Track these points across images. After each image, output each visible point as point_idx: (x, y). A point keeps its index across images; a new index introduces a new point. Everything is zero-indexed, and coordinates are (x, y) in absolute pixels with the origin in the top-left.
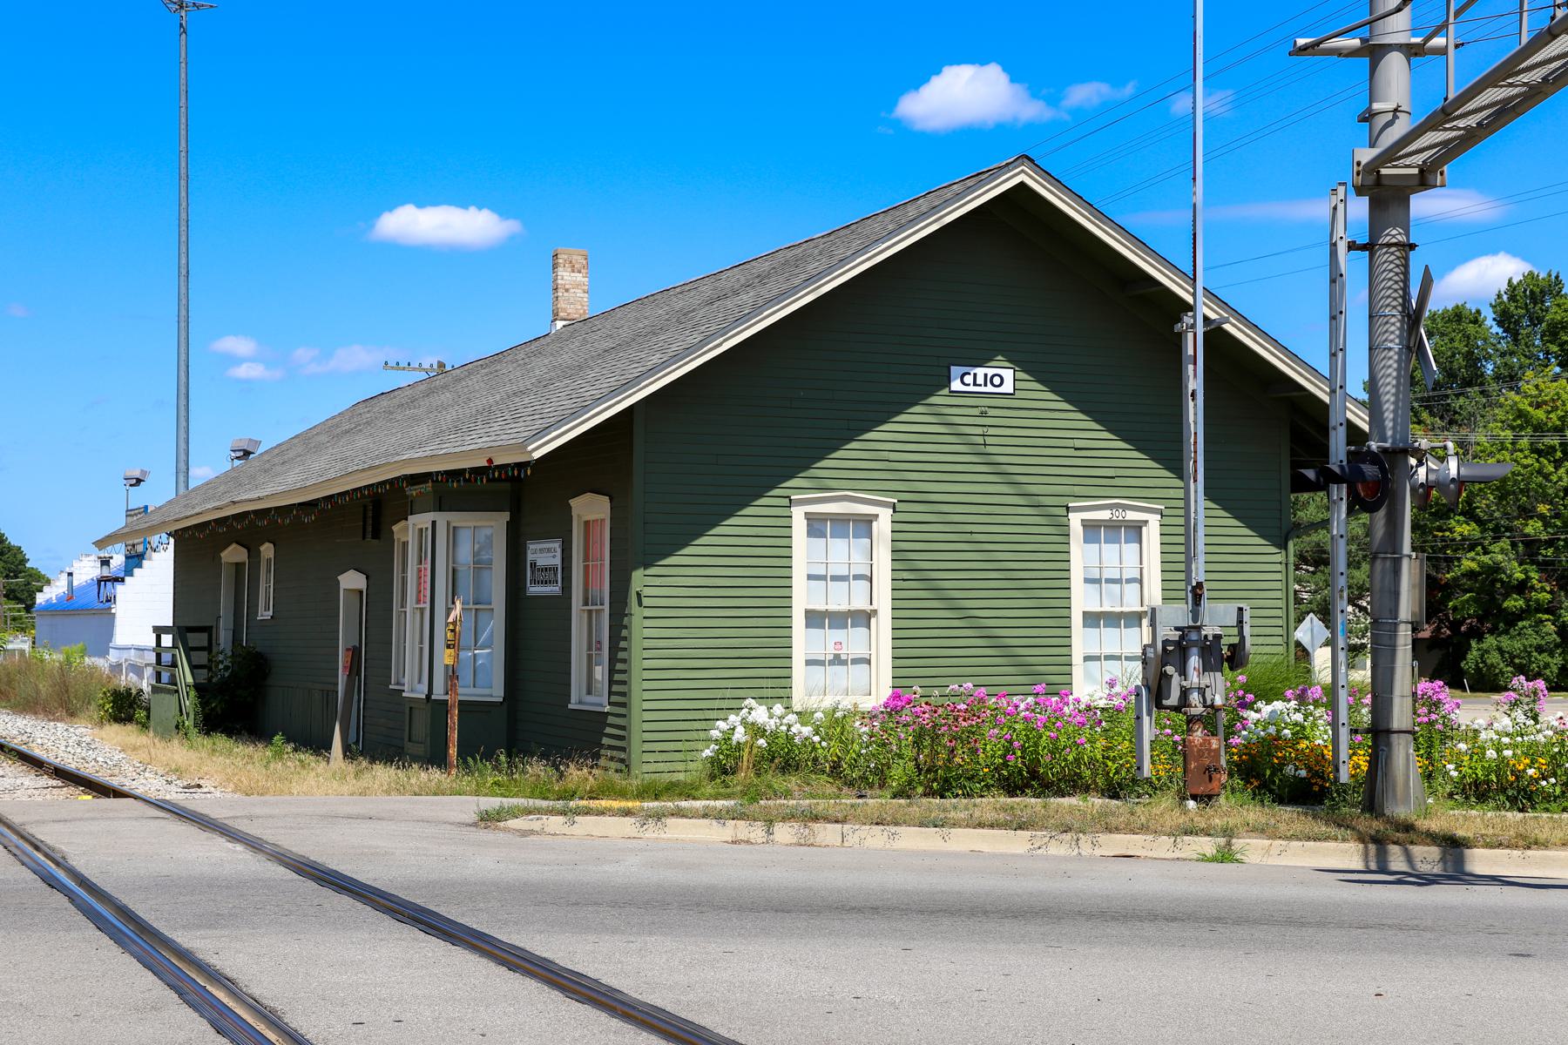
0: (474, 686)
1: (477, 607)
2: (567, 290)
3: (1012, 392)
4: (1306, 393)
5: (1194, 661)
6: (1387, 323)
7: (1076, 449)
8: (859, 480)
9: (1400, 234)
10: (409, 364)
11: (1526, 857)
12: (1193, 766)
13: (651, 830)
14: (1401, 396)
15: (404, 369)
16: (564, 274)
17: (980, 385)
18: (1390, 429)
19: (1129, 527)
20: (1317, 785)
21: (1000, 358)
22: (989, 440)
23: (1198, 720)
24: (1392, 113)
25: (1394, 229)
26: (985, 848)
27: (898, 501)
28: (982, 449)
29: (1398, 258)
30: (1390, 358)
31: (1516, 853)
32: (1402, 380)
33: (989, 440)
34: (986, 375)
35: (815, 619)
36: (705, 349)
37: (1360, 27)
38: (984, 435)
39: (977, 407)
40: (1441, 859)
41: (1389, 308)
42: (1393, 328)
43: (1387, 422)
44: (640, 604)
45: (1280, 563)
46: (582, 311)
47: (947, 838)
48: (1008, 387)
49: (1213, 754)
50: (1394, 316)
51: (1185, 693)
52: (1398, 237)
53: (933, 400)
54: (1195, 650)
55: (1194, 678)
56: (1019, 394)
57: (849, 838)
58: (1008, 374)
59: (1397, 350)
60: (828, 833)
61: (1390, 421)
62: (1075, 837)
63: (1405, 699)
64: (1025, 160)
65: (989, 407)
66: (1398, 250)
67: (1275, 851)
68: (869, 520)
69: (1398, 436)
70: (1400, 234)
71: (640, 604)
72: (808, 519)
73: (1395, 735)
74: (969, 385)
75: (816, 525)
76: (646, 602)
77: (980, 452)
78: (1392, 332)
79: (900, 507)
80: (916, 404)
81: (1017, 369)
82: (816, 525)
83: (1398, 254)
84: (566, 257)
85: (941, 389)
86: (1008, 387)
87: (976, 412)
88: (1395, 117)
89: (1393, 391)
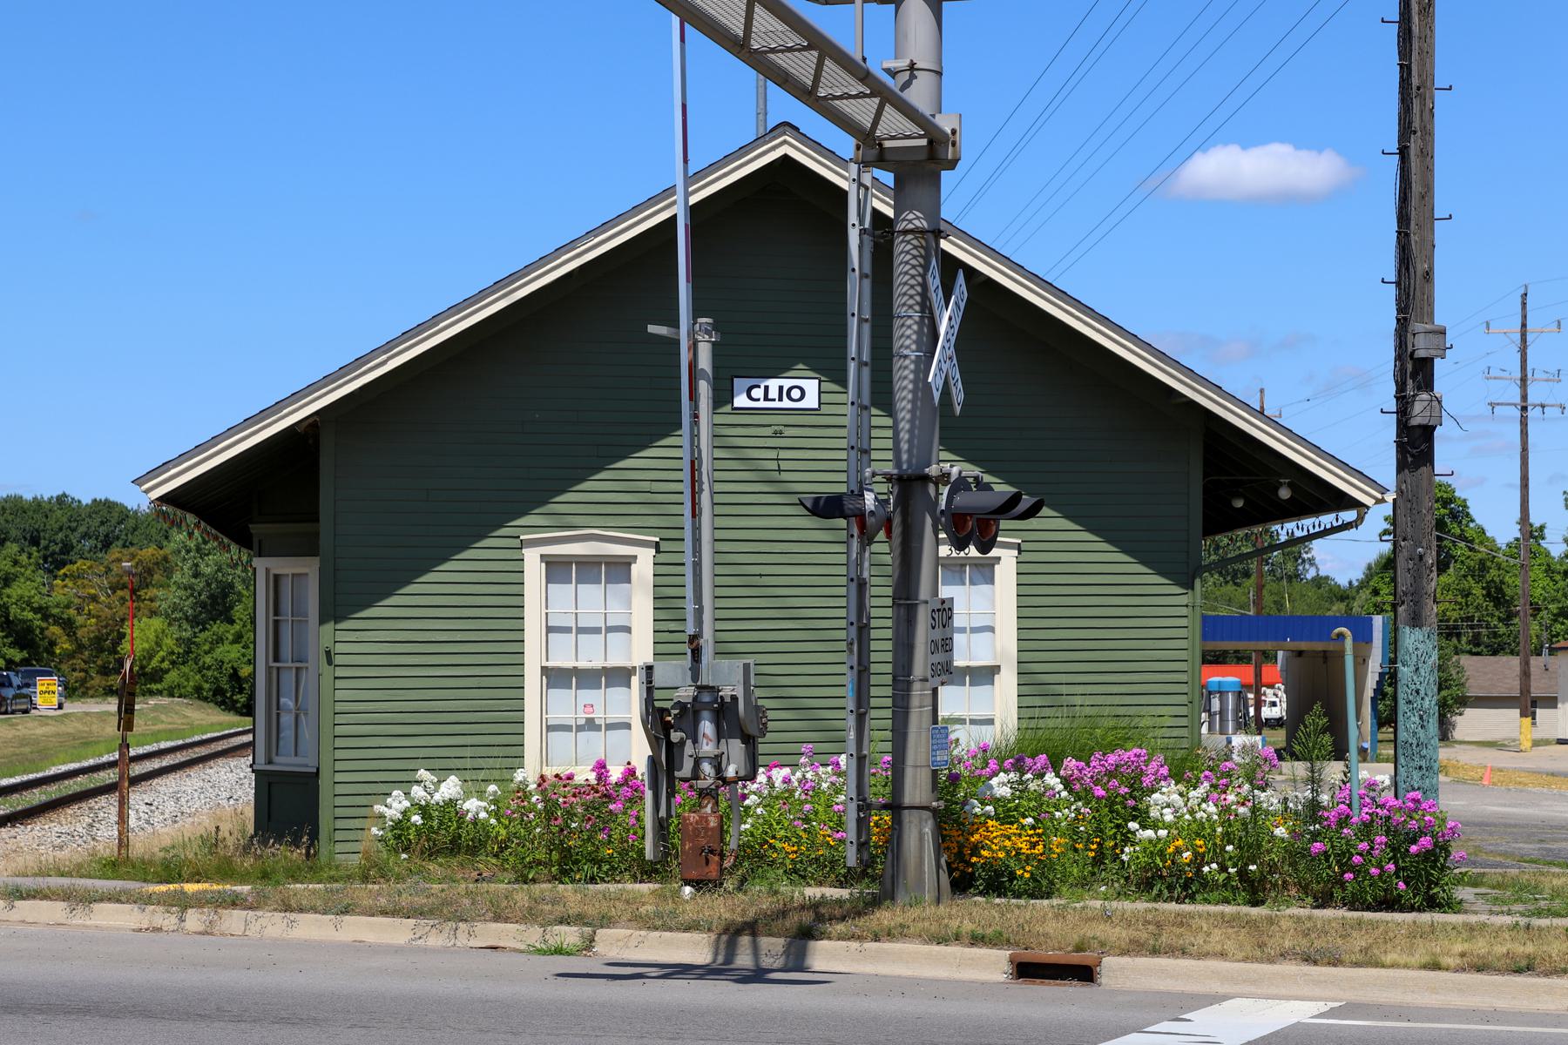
0: (296, 755)
1: (298, 665)
4: (1184, 400)
5: (707, 727)
6: (903, 325)
8: (611, 515)
9: (918, 218)
11: (863, 951)
12: (687, 847)
13: (78, 916)
14: (918, 413)
17: (774, 400)
18: (905, 452)
19: (976, 565)
20: (958, 870)
21: (801, 366)
22: (784, 465)
23: (707, 794)
24: (908, 72)
25: (911, 212)
26: (370, 937)
27: (660, 539)
29: (915, 247)
30: (906, 367)
31: (854, 945)
32: (920, 394)
33: (784, 465)
34: (781, 388)
35: (555, 677)
36: (364, 369)
38: (777, 459)
39: (770, 426)
40: (784, 952)
41: (905, 308)
42: (909, 332)
43: (902, 444)
44: (330, 662)
45: (1187, 606)
47: (339, 926)
48: (811, 401)
49: (710, 833)
50: (910, 317)
51: (697, 762)
52: (917, 222)
54: (706, 714)
55: (708, 748)
56: (825, 409)
57: (251, 926)
58: (811, 386)
59: (913, 358)
60: (234, 920)
61: (905, 442)
62: (454, 926)
63: (919, 769)
64: (787, 128)
65: (785, 426)
66: (916, 238)
67: (633, 942)
68: (628, 562)
69: (914, 461)
70: (918, 218)
71: (330, 662)
72: (547, 564)
73: (906, 812)
74: (759, 400)
75: (556, 569)
76: (338, 660)
78: (908, 337)
79: (1024, 547)
81: (823, 378)
82: (556, 569)
83: (915, 242)
86: (811, 401)
87: (768, 431)
88: (913, 77)
89: (909, 406)
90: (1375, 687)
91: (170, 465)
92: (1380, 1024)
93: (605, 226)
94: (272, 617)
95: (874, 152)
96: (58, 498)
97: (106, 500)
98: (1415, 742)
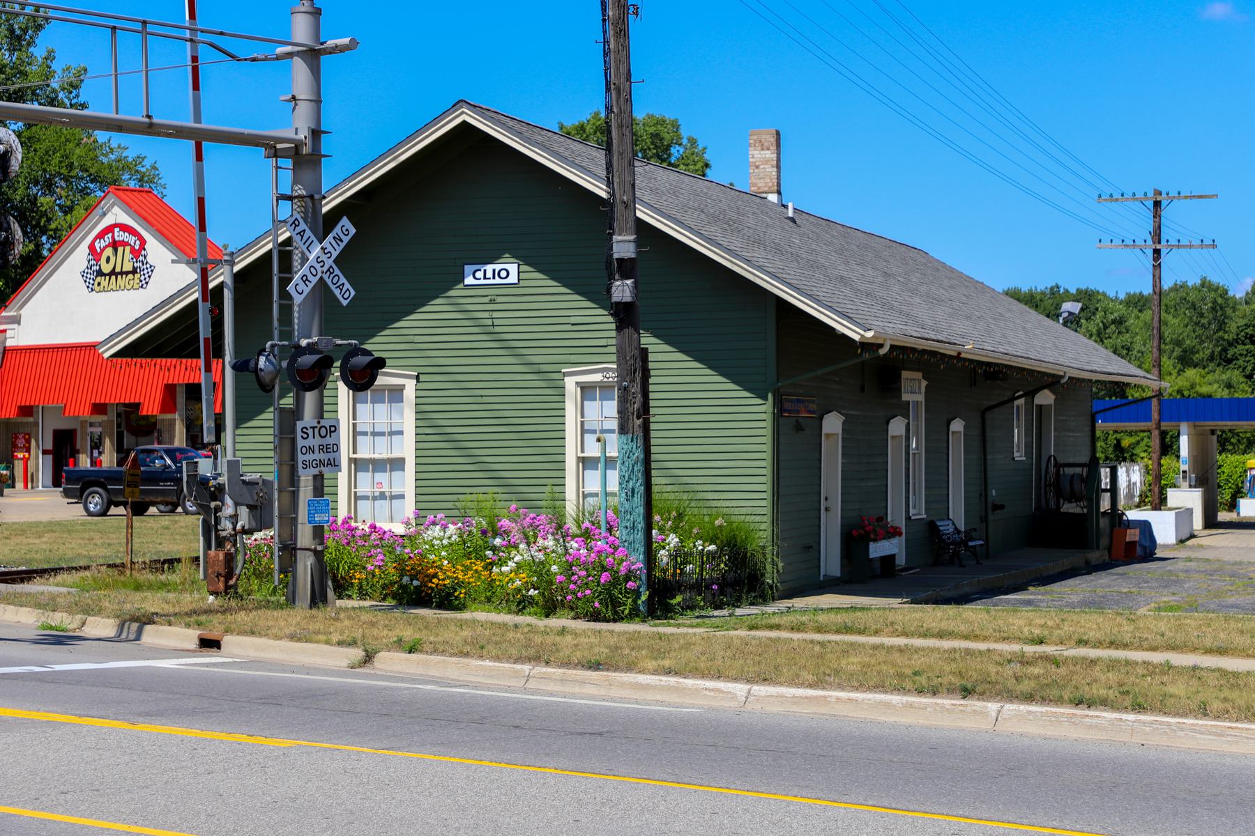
2: (757, 167)
3: (517, 282)
7: (573, 325)
9: (300, 189)
10: (1179, 193)
15: (1117, 200)
16: (755, 152)
21: (507, 255)
28: (491, 329)
33: (496, 322)
34: (494, 270)
37: (221, 51)
46: (771, 184)
48: (513, 278)
52: (299, 191)
53: (451, 293)
64: (464, 103)
70: (300, 189)
77: (490, 331)
80: (437, 297)
83: (298, 203)
84: (756, 137)
85: (458, 284)
86: (513, 278)
87: (486, 300)
90: (339, 473)
91: (114, 337)
92: (249, 672)
93: (355, 175)
94: (351, 421)
95: (273, 151)
96: (1052, 289)
97: (1204, 283)
98: (623, 510)
